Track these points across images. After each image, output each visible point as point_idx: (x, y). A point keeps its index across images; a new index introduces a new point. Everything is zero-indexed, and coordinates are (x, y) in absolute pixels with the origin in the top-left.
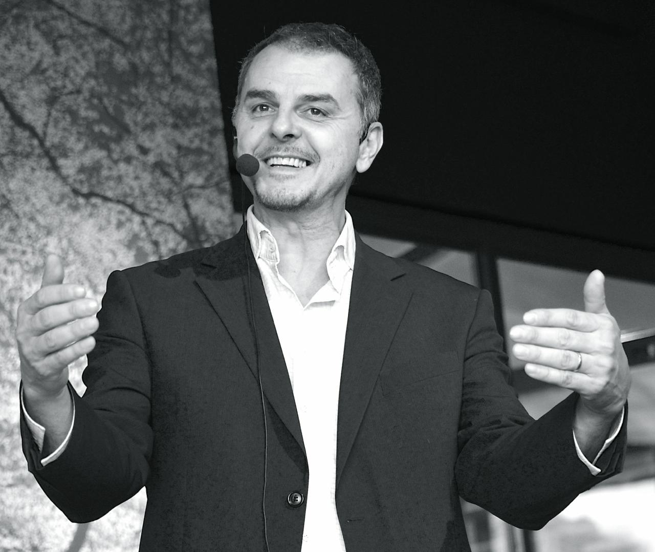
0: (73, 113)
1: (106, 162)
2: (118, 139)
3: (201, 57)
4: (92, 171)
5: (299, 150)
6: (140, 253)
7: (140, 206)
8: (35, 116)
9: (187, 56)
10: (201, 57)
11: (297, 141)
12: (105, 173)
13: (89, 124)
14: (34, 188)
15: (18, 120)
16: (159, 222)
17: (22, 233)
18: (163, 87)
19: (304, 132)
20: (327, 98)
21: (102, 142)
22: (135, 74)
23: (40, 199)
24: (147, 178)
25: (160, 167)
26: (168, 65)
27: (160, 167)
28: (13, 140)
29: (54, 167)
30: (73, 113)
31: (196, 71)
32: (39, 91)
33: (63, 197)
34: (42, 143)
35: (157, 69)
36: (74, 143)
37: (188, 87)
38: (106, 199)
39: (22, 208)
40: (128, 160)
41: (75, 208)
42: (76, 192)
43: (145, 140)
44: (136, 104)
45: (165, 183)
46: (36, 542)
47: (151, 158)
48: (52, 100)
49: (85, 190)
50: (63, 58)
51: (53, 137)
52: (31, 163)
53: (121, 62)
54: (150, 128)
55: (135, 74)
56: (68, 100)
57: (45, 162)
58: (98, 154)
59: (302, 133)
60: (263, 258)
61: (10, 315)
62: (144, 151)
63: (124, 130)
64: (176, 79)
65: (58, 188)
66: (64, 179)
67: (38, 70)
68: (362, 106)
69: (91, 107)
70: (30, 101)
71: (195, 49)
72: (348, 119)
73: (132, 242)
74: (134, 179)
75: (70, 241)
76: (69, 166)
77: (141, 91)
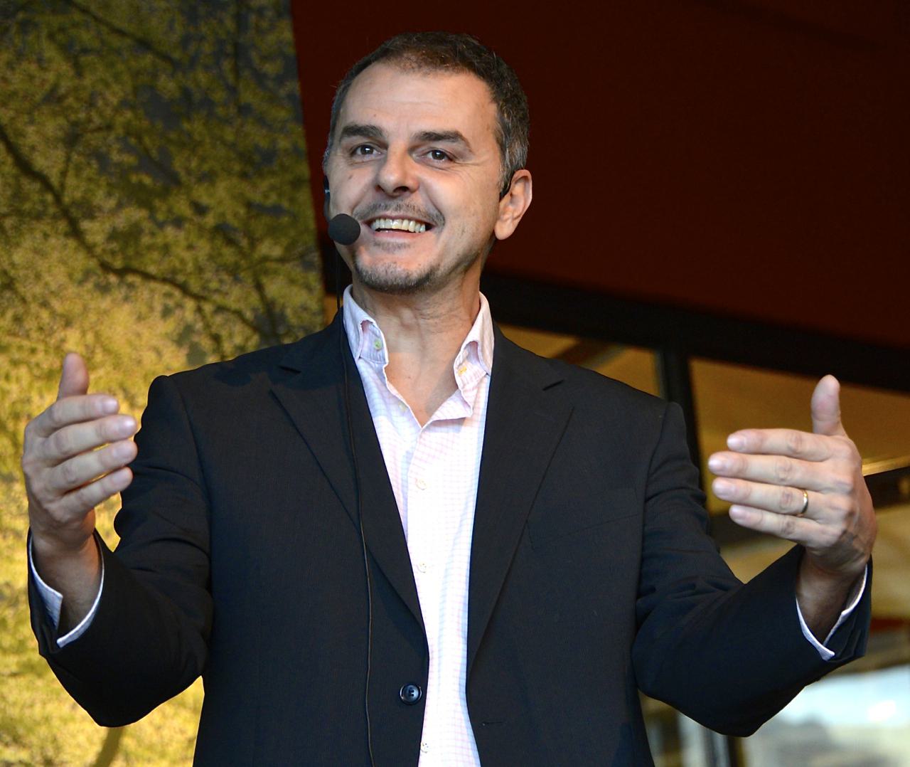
0: (102, 158)
1: (147, 225)
2: (164, 194)
3: (280, 80)
4: (128, 237)
5: (416, 208)
6: (195, 352)
7: (195, 286)
8: (48, 161)
9: (260, 78)
10: (280, 80)
11: (413, 196)
12: (146, 240)
13: (124, 172)
14: (48, 261)
15: (25, 167)
16: (220, 309)
17: (30, 324)
18: (227, 121)
19: (423, 183)
20: (455, 136)
21: (142, 198)
22: (188, 103)
23: (56, 276)
24: (204, 247)
25: (222, 232)
26: (233, 90)
27: (222, 232)
28: (18, 195)
29: (75, 233)
30: (102, 158)
31: (273, 99)
32: (53, 126)
33: (87, 274)
34: (58, 199)
35: (219, 96)
36: (100, 198)
37: (261, 121)
38: (147, 277)
39: (31, 290)
40: (178, 222)
41: (104, 289)
42: (106, 267)
43: (202, 194)
44: (189, 144)
45: (229, 254)
46: (50, 753)
47: (210, 220)
48: (72, 139)
49: (118, 264)
50: (88, 81)
51: (74, 190)
52: (44, 226)
53: (168, 86)
54: (208, 178)
55: (188, 103)
56: (95, 139)
57: (63, 225)
58: (135, 214)
59: (420, 185)
60: (366, 358)
61: (14, 438)
62: (200, 210)
63: (172, 182)
64: (244, 110)
65: (81, 261)
66: (90, 249)
67: (53, 97)
68: (503, 148)
69: (127, 149)
70: (42, 139)
71: (270, 68)
72: (484, 165)
73: (183, 337)
74: (186, 248)
75: (97, 335)
76: (96, 231)
77: (196, 127)
